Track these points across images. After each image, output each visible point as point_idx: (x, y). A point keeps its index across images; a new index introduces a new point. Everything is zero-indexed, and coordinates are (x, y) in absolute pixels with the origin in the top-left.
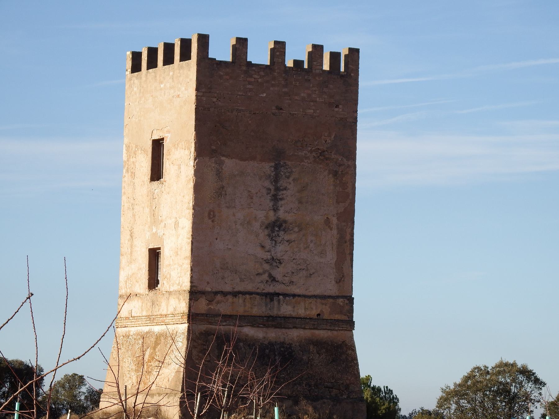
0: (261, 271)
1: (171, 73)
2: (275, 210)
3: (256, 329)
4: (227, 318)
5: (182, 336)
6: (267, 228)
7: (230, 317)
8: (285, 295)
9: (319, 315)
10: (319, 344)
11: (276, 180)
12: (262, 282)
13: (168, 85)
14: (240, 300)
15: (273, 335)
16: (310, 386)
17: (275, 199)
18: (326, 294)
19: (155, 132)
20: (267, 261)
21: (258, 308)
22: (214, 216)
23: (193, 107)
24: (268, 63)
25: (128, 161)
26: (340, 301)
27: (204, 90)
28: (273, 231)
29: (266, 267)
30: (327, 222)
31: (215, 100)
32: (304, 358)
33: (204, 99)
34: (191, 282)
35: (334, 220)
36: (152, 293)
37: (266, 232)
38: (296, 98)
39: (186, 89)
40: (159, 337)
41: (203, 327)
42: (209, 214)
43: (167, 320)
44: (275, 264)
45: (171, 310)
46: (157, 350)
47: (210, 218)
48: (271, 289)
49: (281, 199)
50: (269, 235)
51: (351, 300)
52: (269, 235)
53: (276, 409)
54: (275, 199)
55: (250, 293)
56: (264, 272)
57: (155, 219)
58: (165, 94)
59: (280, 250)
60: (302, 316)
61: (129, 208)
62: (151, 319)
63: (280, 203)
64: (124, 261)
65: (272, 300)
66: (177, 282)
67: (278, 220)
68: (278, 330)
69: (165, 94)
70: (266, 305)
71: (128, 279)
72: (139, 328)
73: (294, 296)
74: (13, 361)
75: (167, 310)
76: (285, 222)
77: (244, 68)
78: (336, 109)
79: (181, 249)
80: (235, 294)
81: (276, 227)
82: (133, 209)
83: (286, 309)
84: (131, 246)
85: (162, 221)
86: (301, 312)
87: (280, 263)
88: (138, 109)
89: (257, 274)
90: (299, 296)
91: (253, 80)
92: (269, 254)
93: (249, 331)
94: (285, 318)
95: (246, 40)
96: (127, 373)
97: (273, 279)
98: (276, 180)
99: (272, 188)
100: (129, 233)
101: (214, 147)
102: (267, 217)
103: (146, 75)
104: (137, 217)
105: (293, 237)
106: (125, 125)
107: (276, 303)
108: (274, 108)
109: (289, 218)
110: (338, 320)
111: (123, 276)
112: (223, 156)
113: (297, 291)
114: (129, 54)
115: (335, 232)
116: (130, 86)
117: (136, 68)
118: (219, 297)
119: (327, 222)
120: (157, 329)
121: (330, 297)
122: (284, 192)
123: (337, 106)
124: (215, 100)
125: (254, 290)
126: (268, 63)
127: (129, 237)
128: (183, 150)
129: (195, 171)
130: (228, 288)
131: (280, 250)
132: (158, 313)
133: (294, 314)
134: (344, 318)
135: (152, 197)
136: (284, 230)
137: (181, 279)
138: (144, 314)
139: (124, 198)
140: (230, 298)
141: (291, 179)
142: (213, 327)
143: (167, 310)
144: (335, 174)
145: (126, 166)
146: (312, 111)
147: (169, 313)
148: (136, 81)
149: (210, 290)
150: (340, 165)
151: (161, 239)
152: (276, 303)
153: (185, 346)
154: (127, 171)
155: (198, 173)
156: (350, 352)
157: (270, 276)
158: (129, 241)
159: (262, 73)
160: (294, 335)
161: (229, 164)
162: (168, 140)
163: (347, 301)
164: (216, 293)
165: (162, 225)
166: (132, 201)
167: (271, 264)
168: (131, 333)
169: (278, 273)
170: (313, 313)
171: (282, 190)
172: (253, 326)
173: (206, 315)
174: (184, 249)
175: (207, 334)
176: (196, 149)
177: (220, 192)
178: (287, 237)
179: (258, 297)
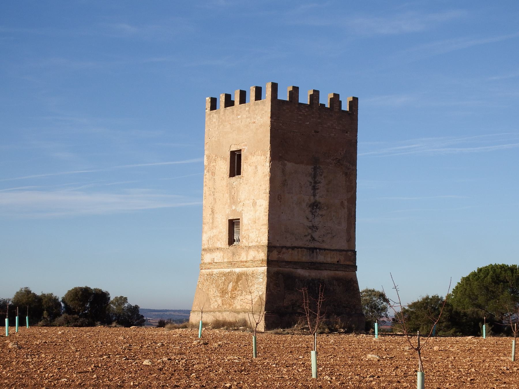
0: (307, 234)
1: (247, 109)
2: (314, 195)
3: (304, 270)
4: (288, 263)
5: (262, 275)
6: (310, 206)
7: (290, 262)
8: (320, 249)
9: (338, 262)
10: (338, 280)
11: (315, 177)
12: (307, 241)
13: (245, 116)
14: (295, 252)
15: (314, 274)
16: (335, 306)
17: (314, 188)
18: (342, 249)
19: (233, 146)
20: (310, 228)
21: (305, 258)
22: (281, 199)
23: (269, 128)
24: (308, 103)
25: (209, 165)
26: (349, 253)
27: (275, 118)
28: (313, 209)
29: (310, 231)
30: (342, 203)
31: (281, 125)
32: (331, 288)
33: (275, 124)
34: (268, 240)
35: (346, 203)
36: (232, 248)
37: (310, 209)
38: (325, 126)
39: (261, 118)
40: (239, 277)
41: (275, 269)
42: (278, 197)
43: (247, 265)
44: (314, 229)
45: (250, 258)
46: (239, 284)
47: (278, 200)
48: (312, 245)
49: (318, 189)
50: (311, 211)
51: (355, 253)
52: (311, 211)
53: (6, 320)
54: (314, 188)
55: (301, 248)
56: (308, 235)
57: (234, 200)
58: (241, 122)
59: (317, 221)
60: (329, 262)
61: (210, 195)
62: (231, 264)
63: (317, 191)
64: (206, 228)
65: (313, 252)
66: (256, 240)
67: (316, 202)
68: (316, 271)
69: (241, 122)
70: (310, 255)
71: (210, 238)
72: (221, 270)
73: (325, 249)
74: (44, 295)
75: (247, 258)
76: (320, 203)
77: (297, 106)
78: (346, 134)
79: (259, 219)
80: (293, 248)
81: (315, 206)
82: (214, 195)
83: (321, 258)
84: (213, 218)
85: (240, 202)
86: (329, 260)
87: (317, 229)
88: (217, 133)
89: (305, 236)
90: (327, 250)
91: (302, 113)
92: (311, 223)
93: (301, 272)
94: (321, 264)
95: (298, 88)
96: (212, 298)
97: (313, 239)
98: (315, 177)
99: (313, 181)
100: (211, 210)
101: (280, 155)
102: (310, 200)
103: (224, 111)
104: (217, 200)
105: (324, 213)
106: (205, 143)
107: (315, 254)
108: (313, 131)
109: (322, 200)
110: (348, 265)
111: (205, 237)
112: (286, 160)
113: (326, 247)
114: (208, 99)
115: (346, 210)
116: (210, 119)
117: (214, 106)
118: (284, 250)
119: (342, 203)
120: (237, 270)
121: (344, 250)
122: (319, 184)
123: (347, 132)
124: (281, 125)
125: (303, 246)
126: (308, 103)
127: (210, 212)
128: (260, 157)
129: (270, 169)
130: (288, 244)
131: (317, 221)
132: (238, 260)
133: (325, 261)
134: (351, 263)
135: (231, 188)
136: (319, 208)
137: (259, 239)
138: (226, 260)
139: (205, 189)
140: (290, 251)
141: (323, 176)
142: (281, 269)
143: (247, 258)
144: (346, 174)
145: (207, 168)
146: (333, 135)
147: (248, 260)
148: (215, 115)
149: (279, 245)
150: (348, 169)
151: (241, 213)
152: (315, 254)
153: (266, 281)
154: (208, 171)
155: (272, 171)
156: (355, 285)
157: (312, 237)
158: (210, 215)
159: (307, 110)
160: (325, 274)
161: (289, 165)
162: (245, 151)
163: (353, 253)
164: (282, 247)
165: (241, 204)
166: (213, 190)
167: (312, 230)
168: (214, 273)
169: (316, 235)
170: (335, 260)
171: (318, 183)
172: (303, 268)
173: (277, 261)
174: (262, 219)
175: (277, 273)
176: (271, 155)
177: (284, 183)
178: (320, 213)
179: (305, 250)
